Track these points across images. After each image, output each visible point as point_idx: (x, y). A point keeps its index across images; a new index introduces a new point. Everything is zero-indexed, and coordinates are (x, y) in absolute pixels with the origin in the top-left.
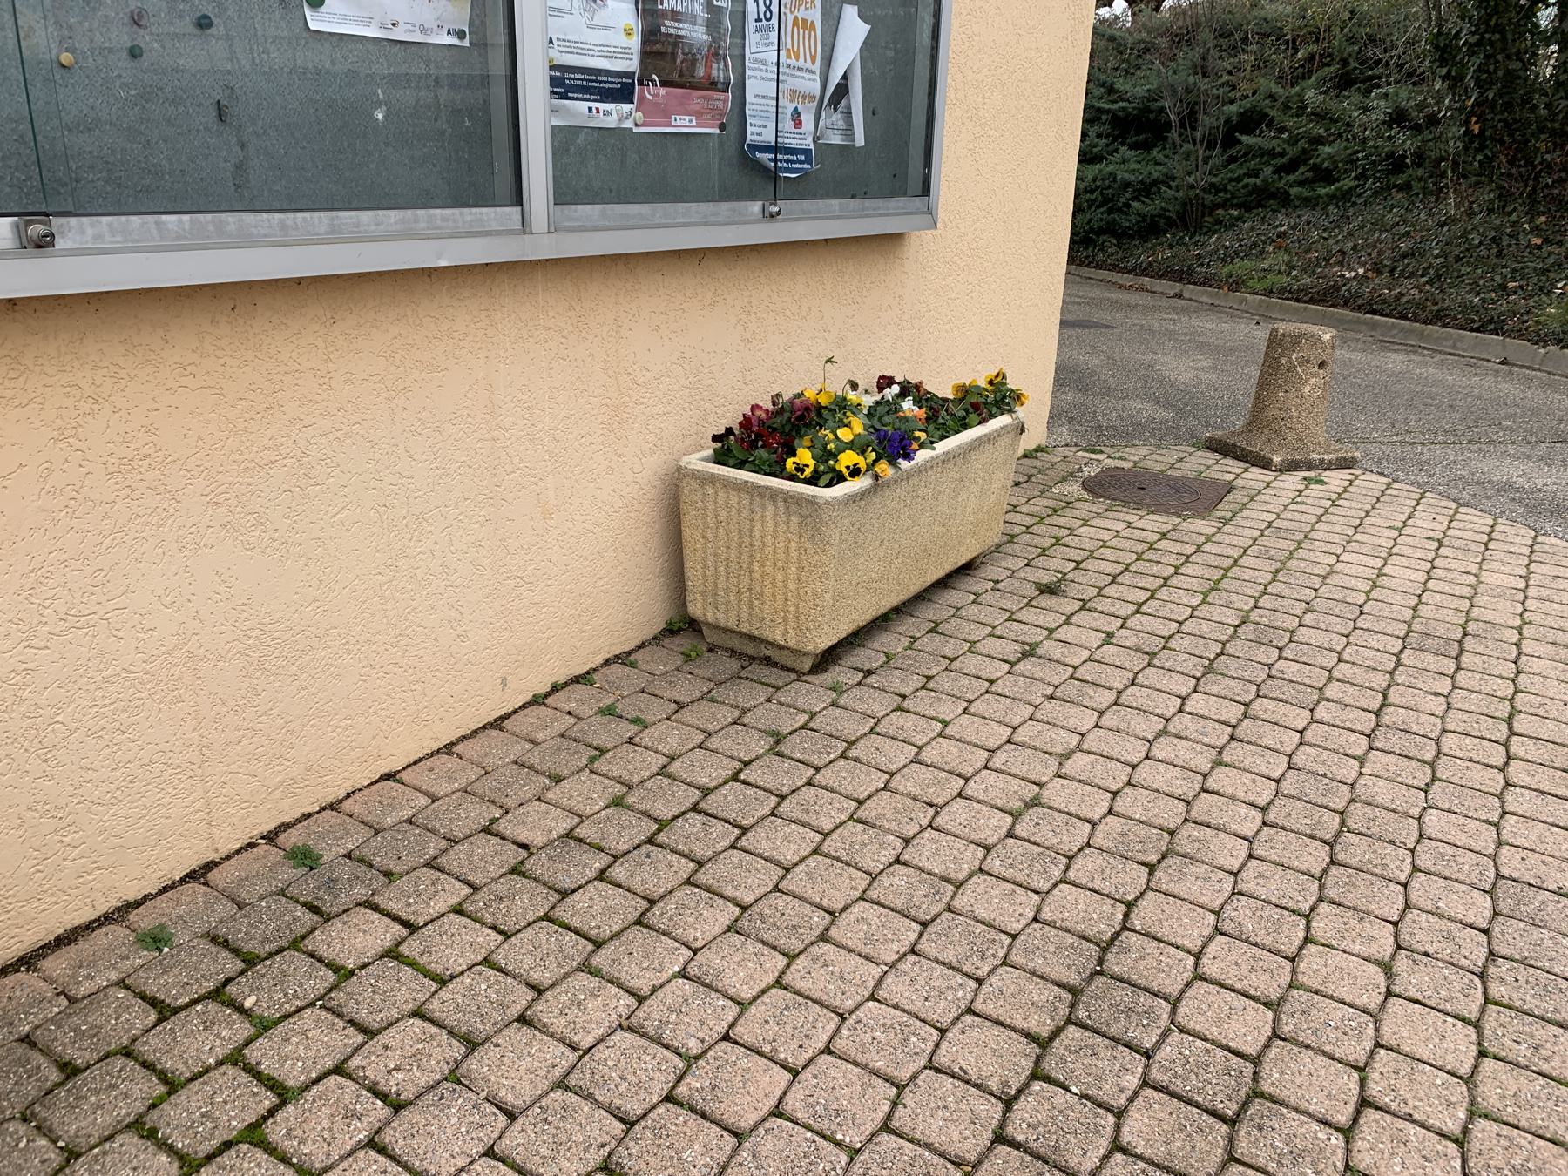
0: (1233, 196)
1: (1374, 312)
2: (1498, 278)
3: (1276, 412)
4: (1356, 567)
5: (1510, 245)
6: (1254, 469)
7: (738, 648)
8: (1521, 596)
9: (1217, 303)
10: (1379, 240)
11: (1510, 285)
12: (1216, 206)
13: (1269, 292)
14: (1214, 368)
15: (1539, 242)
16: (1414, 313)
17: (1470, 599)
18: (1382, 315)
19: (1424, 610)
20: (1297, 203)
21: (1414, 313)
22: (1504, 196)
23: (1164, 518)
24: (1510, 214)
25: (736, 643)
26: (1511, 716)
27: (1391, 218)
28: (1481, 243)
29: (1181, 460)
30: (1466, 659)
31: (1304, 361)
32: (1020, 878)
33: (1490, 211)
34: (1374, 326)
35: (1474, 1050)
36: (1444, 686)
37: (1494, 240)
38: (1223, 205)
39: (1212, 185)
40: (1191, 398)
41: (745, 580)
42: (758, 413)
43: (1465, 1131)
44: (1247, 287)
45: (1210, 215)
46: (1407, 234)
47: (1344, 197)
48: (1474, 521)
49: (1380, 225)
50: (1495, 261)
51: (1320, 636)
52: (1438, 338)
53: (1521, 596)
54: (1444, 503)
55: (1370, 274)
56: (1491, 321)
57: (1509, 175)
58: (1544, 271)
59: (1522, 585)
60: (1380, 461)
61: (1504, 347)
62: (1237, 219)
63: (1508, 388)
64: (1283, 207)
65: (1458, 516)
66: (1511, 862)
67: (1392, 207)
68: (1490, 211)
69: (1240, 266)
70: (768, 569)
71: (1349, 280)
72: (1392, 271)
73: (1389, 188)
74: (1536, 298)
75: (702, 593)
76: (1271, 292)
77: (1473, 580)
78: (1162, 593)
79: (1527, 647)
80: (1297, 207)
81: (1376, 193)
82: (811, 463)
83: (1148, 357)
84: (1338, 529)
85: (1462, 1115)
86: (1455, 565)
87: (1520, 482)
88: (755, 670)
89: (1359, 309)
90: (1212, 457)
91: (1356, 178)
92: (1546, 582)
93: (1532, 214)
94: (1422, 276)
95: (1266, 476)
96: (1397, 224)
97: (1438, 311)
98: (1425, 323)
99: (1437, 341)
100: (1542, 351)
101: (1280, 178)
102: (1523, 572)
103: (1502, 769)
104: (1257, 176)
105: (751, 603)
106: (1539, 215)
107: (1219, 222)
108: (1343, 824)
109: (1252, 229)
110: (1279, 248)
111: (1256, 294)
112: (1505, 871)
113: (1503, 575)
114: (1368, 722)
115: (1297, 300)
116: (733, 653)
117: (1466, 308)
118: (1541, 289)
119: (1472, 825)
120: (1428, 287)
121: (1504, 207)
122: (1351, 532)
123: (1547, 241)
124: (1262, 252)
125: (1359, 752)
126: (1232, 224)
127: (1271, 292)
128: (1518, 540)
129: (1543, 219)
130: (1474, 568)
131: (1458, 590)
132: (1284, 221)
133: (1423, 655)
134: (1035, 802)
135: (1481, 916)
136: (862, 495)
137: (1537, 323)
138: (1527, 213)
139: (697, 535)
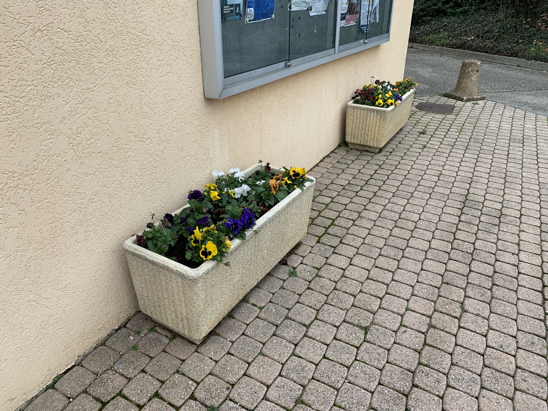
0: (428, 13)
1: (477, 51)
2: (516, 39)
3: (464, 85)
4: (494, 125)
5: (519, 28)
6: (458, 101)
7: (358, 149)
8: (535, 130)
9: (425, 49)
10: (477, 27)
11: (520, 41)
12: (423, 16)
13: (443, 45)
14: (434, 71)
15: (528, 27)
16: (490, 51)
17: (523, 131)
18: (480, 52)
19: (512, 134)
20: (449, 14)
21: (490, 51)
22: (518, 12)
23: (441, 115)
24: (519, 18)
25: (358, 147)
26: (537, 155)
27: (481, 19)
28: (510, 28)
29: (438, 100)
30: (525, 144)
31: (472, 70)
32: (445, 186)
33: (513, 17)
34: (477, 55)
35: (540, 207)
36: (521, 149)
37: (514, 27)
38: (425, 16)
39: (422, 9)
40: (432, 82)
41: (363, 131)
42: (359, 91)
43: (540, 217)
44: (435, 44)
45: (421, 19)
46: (486, 25)
47: (465, 12)
48: (520, 113)
49: (477, 22)
50: (515, 33)
51: (490, 140)
52: (497, 59)
53: (535, 130)
54: (511, 108)
55: (475, 39)
56: (514, 53)
57: (520, 5)
58: (530, 36)
59: (535, 127)
60: (491, 98)
61: (518, 61)
62: (430, 20)
63: (521, 74)
64: (445, 16)
65: (516, 111)
66: (541, 180)
67: (481, 15)
68: (513, 17)
69: (432, 37)
70: (370, 128)
71: (469, 41)
72: (482, 37)
73: (480, 9)
74: (528, 45)
75: (351, 136)
76: (443, 45)
77: (523, 126)
78: (449, 133)
79: (538, 140)
80: (449, 15)
81: (475, 11)
82: (382, 103)
83: (413, 69)
84: (486, 116)
85: (539, 215)
86: (518, 123)
87: (530, 102)
88: (363, 153)
89: (472, 50)
90: (446, 99)
91: (469, 6)
92: (541, 126)
93: (526, 18)
94: (492, 39)
95: (463, 103)
96: (483, 21)
97: (498, 50)
98: (494, 54)
99: (497, 60)
100: (530, 62)
101: (444, 6)
102: (535, 124)
103: (537, 164)
104: (436, 5)
105: (364, 137)
106: (528, 18)
107: (423, 21)
108: (506, 175)
109: (435, 24)
110: (445, 30)
111: (438, 46)
112: (541, 182)
113: (530, 125)
114: (506, 157)
115: (452, 48)
116: (357, 150)
117: (506, 49)
118: (529, 42)
119: (532, 174)
120: (494, 43)
121: (518, 16)
122: (490, 116)
123: (531, 26)
124: (439, 32)
125: (506, 163)
126: (428, 22)
127: (443, 45)
128: (532, 116)
129: (529, 19)
130: (522, 124)
131: (520, 129)
132: (445, 20)
133: (515, 143)
134: (441, 174)
135: (538, 189)
136: (393, 110)
137: (528, 53)
138: (525, 18)
139: (351, 121)
